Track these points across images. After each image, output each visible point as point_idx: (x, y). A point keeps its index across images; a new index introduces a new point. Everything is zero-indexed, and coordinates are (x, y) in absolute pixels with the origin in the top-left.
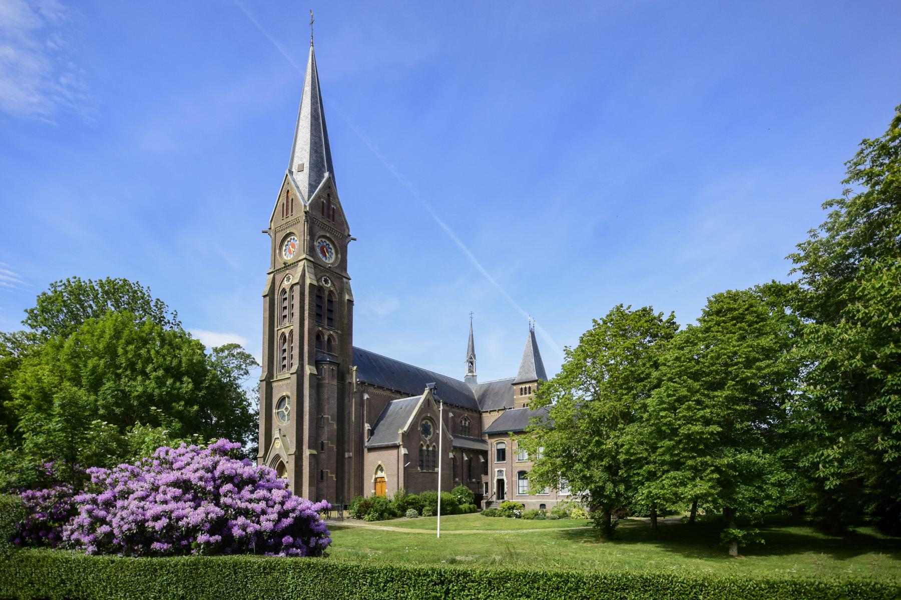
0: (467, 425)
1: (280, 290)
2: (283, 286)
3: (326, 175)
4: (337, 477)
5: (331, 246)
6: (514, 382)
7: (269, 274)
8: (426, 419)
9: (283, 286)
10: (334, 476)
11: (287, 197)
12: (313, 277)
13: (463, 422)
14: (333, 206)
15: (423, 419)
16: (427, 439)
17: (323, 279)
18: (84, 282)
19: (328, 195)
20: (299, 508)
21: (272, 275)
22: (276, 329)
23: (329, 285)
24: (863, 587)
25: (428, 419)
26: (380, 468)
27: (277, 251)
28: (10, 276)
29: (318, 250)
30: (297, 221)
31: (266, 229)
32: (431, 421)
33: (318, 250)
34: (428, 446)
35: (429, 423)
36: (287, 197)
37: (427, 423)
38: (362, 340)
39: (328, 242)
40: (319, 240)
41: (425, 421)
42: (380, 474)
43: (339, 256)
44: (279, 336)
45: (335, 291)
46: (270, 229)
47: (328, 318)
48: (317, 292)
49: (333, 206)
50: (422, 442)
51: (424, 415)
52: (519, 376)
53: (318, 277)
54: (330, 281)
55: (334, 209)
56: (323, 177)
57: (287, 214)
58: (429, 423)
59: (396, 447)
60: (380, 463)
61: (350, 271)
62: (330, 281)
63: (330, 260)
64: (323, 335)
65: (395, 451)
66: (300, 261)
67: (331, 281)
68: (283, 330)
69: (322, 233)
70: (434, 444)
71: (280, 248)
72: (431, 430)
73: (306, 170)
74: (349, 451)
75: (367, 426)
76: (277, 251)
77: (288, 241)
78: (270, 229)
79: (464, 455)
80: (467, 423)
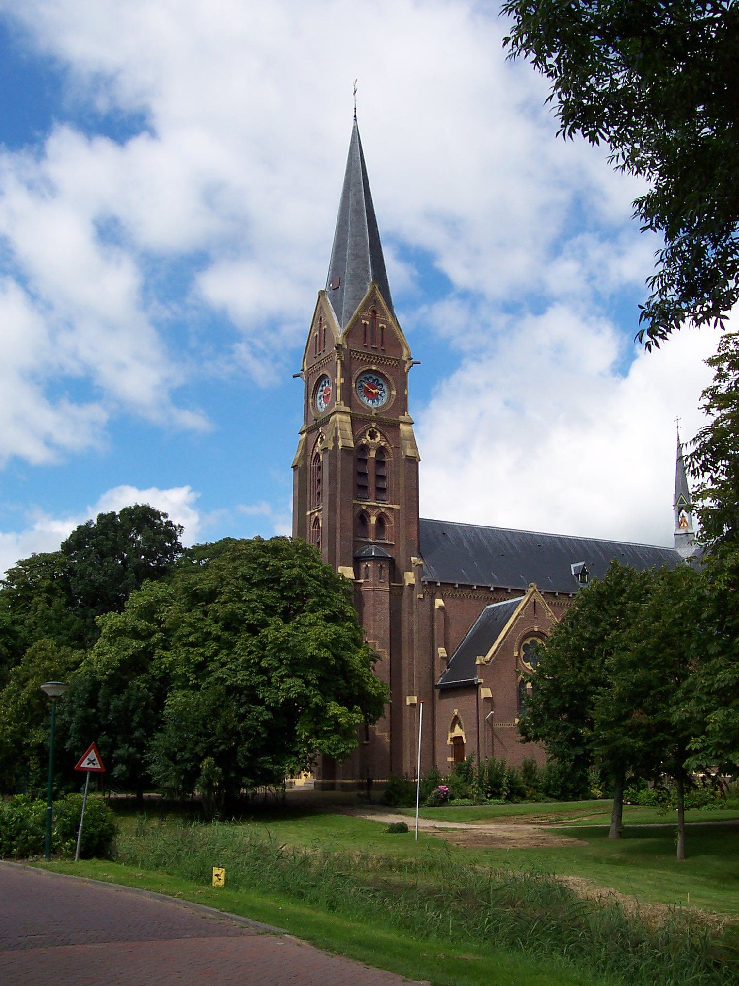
1: (314, 456)
4: (391, 737)
5: (381, 382)
7: (301, 433)
8: (532, 636)
10: (386, 734)
14: (381, 325)
17: (368, 433)
18: (698, 518)
19: (374, 312)
20: (557, 699)
23: (378, 439)
24: (692, 311)
25: (535, 636)
26: (456, 720)
27: (311, 401)
28: (385, 504)
39: (375, 377)
46: (303, 370)
49: (381, 325)
51: (526, 630)
54: (378, 434)
55: (382, 328)
60: (456, 712)
62: (378, 434)
66: (332, 414)
67: (381, 433)
68: (316, 514)
71: (314, 397)
74: (411, 694)
77: (323, 386)
78: (303, 370)
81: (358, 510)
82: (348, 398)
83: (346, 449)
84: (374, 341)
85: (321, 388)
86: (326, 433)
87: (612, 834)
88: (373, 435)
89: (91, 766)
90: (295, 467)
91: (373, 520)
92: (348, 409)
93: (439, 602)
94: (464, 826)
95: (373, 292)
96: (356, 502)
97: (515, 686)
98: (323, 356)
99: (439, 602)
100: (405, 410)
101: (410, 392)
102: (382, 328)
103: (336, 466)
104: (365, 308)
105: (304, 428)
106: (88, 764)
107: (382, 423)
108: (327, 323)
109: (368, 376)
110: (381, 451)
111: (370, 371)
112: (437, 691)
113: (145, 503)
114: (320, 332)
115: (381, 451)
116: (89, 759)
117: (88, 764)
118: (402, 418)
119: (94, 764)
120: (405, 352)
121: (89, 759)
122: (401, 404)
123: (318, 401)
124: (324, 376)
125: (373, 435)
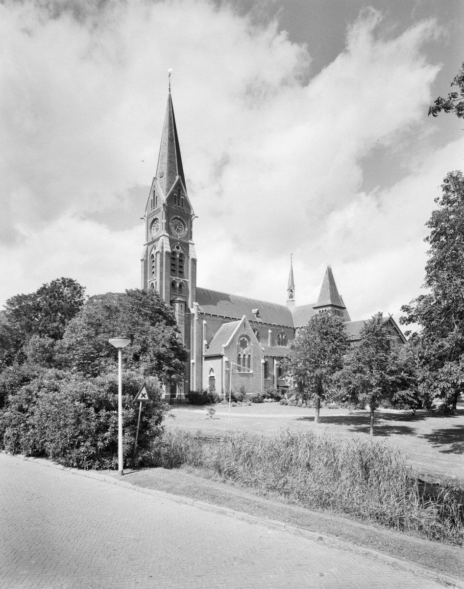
0: (283, 338)
2: (152, 253)
3: (177, 177)
5: (181, 224)
6: (315, 306)
9: (152, 253)
11: (154, 195)
12: (169, 246)
13: (280, 336)
15: (241, 337)
16: (244, 351)
19: (179, 190)
21: (146, 246)
22: (148, 281)
23: (180, 250)
27: (149, 230)
29: (173, 228)
30: (159, 210)
31: (143, 217)
32: (247, 338)
33: (173, 228)
34: (244, 355)
35: (246, 339)
36: (154, 195)
37: (244, 339)
38: (204, 280)
39: (179, 221)
40: (173, 221)
41: (242, 338)
42: (212, 374)
43: (187, 229)
44: (150, 285)
45: (184, 253)
47: (180, 272)
48: (172, 256)
50: (240, 353)
51: (239, 335)
52: (318, 301)
53: (172, 246)
56: (175, 179)
57: (154, 206)
58: (246, 339)
59: (221, 357)
61: (104, 293)
63: (180, 235)
64: (176, 283)
65: (220, 360)
66: (161, 236)
69: (175, 216)
70: (249, 354)
71: (150, 232)
72: (248, 344)
73: (165, 176)
74: (193, 359)
75: (205, 342)
76: (149, 230)
79: (275, 361)
80: (284, 336)
81: (172, 280)
82: (168, 229)
83: (167, 253)
84: (179, 205)
85: (154, 225)
86: (158, 245)
87: (316, 419)
88: (178, 248)
89: (143, 398)
90: (142, 260)
91: (178, 285)
92: (168, 235)
93: (204, 322)
94: (240, 415)
95: (179, 180)
96: (171, 277)
97: (237, 356)
98: (156, 209)
99: (204, 322)
100: (191, 238)
101: (193, 230)
102: (182, 199)
103: (162, 259)
104: (175, 188)
105: (146, 243)
106: (142, 397)
107: (182, 243)
108: (158, 193)
109: (176, 220)
110: (181, 255)
111: (177, 218)
112: (204, 358)
113: (335, 62)
114: (154, 198)
115: (181, 255)
116: (142, 394)
117: (142, 397)
118: (190, 241)
119: (145, 397)
120: (192, 211)
121: (142, 394)
122: (190, 235)
123: (153, 231)
124: (156, 219)
125: (178, 248)
